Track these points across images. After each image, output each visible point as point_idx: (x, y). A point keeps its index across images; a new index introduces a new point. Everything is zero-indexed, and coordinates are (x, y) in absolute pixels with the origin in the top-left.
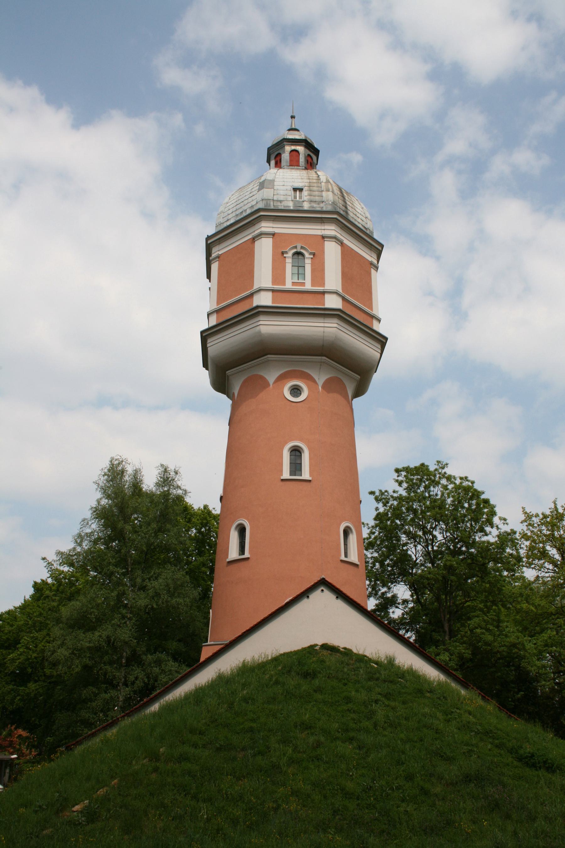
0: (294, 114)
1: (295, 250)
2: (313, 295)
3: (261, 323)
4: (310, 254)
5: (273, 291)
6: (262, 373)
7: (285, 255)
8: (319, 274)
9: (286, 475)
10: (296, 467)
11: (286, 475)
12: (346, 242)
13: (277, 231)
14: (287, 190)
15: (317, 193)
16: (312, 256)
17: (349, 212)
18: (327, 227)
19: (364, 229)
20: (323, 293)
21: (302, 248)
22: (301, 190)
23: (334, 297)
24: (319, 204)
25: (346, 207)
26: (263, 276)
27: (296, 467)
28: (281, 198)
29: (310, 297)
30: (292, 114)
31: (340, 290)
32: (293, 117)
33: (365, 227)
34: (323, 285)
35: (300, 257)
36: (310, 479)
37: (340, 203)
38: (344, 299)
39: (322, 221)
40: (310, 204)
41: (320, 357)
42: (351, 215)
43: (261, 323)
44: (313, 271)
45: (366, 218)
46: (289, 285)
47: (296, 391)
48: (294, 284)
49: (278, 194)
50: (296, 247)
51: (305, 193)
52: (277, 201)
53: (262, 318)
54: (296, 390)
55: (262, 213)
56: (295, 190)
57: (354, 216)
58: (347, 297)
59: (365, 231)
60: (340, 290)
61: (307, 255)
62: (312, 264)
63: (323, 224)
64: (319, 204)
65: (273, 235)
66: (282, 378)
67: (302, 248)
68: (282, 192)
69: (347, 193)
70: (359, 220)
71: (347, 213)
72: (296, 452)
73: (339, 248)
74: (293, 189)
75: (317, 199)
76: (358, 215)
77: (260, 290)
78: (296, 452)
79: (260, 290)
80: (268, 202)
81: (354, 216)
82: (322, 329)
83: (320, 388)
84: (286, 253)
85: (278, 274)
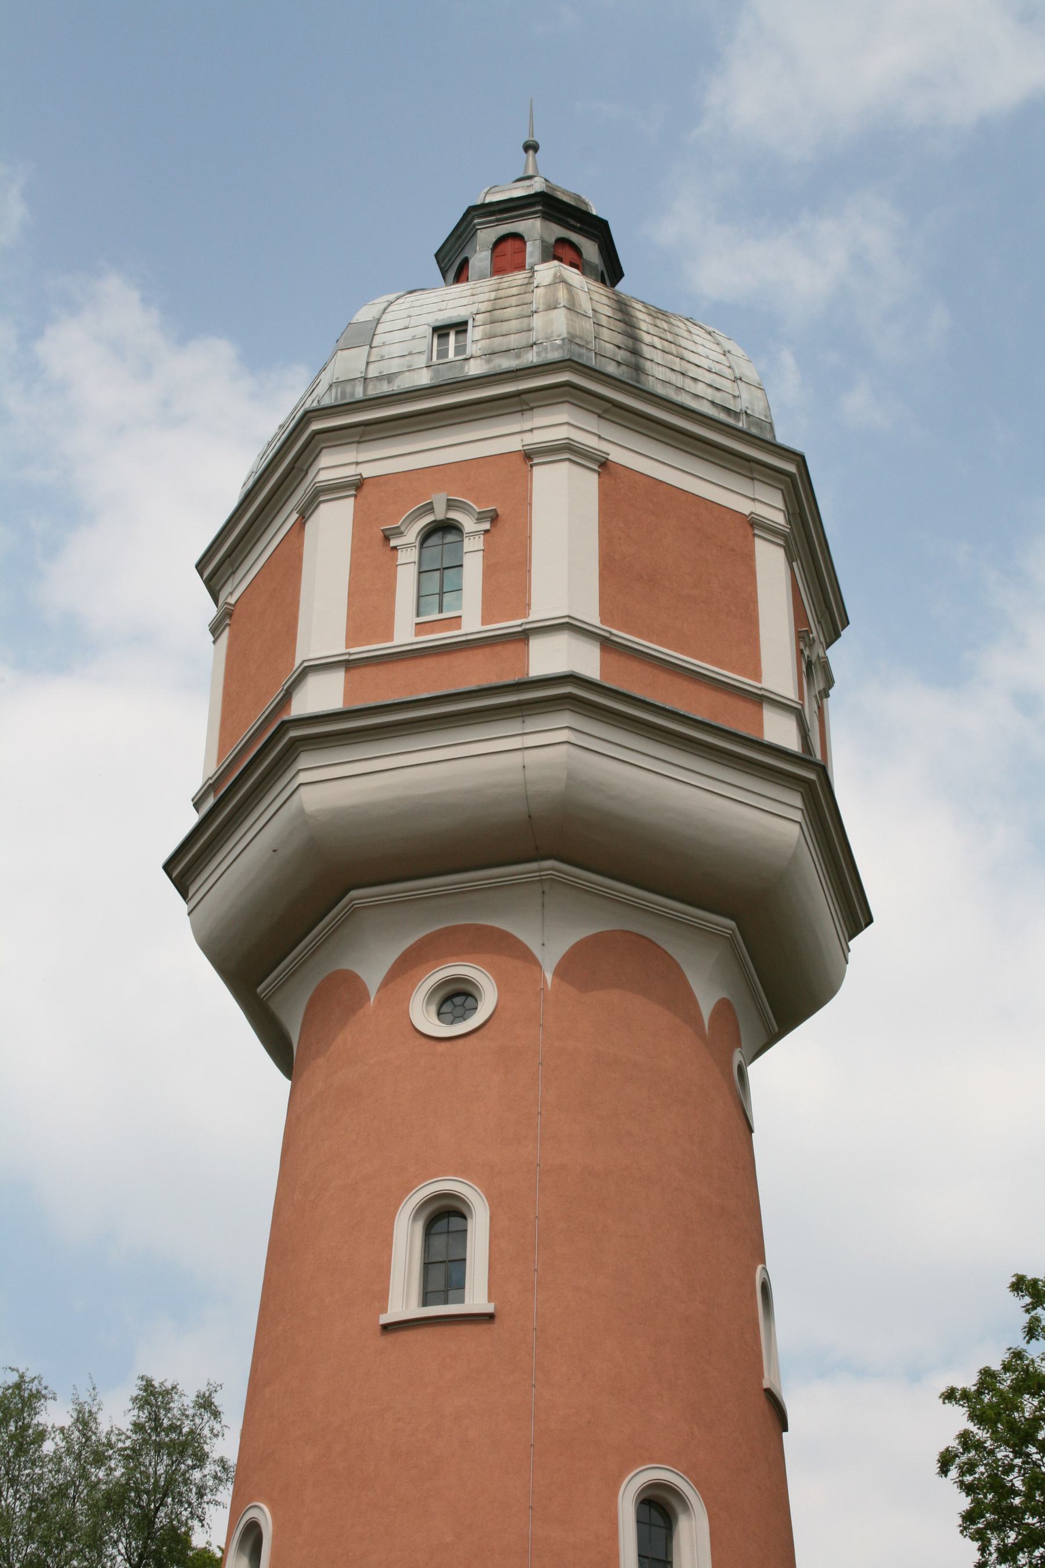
0: (537, 138)
1: (429, 519)
2: (487, 651)
3: (303, 777)
4: (480, 518)
5: (348, 665)
6: (347, 964)
7: (393, 543)
8: (509, 576)
9: (403, 1301)
10: (442, 1274)
11: (403, 1301)
12: (617, 455)
13: (367, 471)
14: (414, 338)
15: (514, 324)
16: (487, 526)
17: (648, 365)
18: (541, 418)
19: (722, 416)
20: (523, 636)
21: (451, 504)
22: (460, 327)
23: (563, 640)
24: (518, 356)
25: (635, 352)
26: (323, 625)
27: (442, 1274)
28: (394, 366)
29: (479, 656)
30: (526, 138)
31: (590, 614)
32: (531, 147)
33: (728, 411)
34: (525, 606)
35: (450, 538)
36: (490, 1308)
37: (610, 338)
38: (607, 644)
39: (520, 403)
40: (488, 361)
41: (534, 866)
42: (658, 374)
43: (303, 777)
44: (490, 571)
45: (737, 379)
46: (404, 634)
47: (456, 997)
48: (421, 627)
49: (382, 359)
50: (429, 508)
51: (474, 333)
52: (380, 378)
53: (305, 760)
54: (458, 1000)
55: (316, 426)
56: (441, 331)
57: (677, 380)
58: (622, 635)
59: (731, 421)
60: (590, 614)
61: (468, 524)
62: (487, 552)
63: (527, 414)
64: (518, 356)
65: (358, 485)
66: (409, 964)
67: (451, 504)
68: (396, 350)
69: (658, 314)
70: (700, 389)
71: (638, 369)
72: (444, 1217)
73: (590, 482)
74: (435, 330)
75: (513, 341)
76: (693, 372)
77: (306, 671)
78: (444, 1217)
79: (306, 671)
80: (348, 388)
81: (677, 380)
82: (516, 758)
83: (549, 977)
84: (398, 532)
85: (368, 604)
